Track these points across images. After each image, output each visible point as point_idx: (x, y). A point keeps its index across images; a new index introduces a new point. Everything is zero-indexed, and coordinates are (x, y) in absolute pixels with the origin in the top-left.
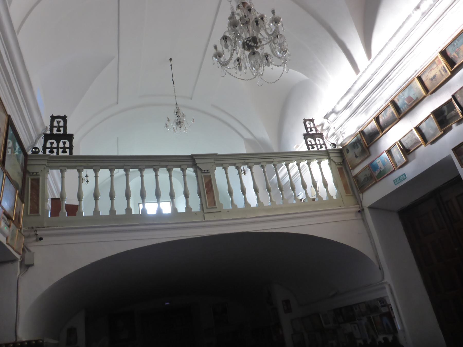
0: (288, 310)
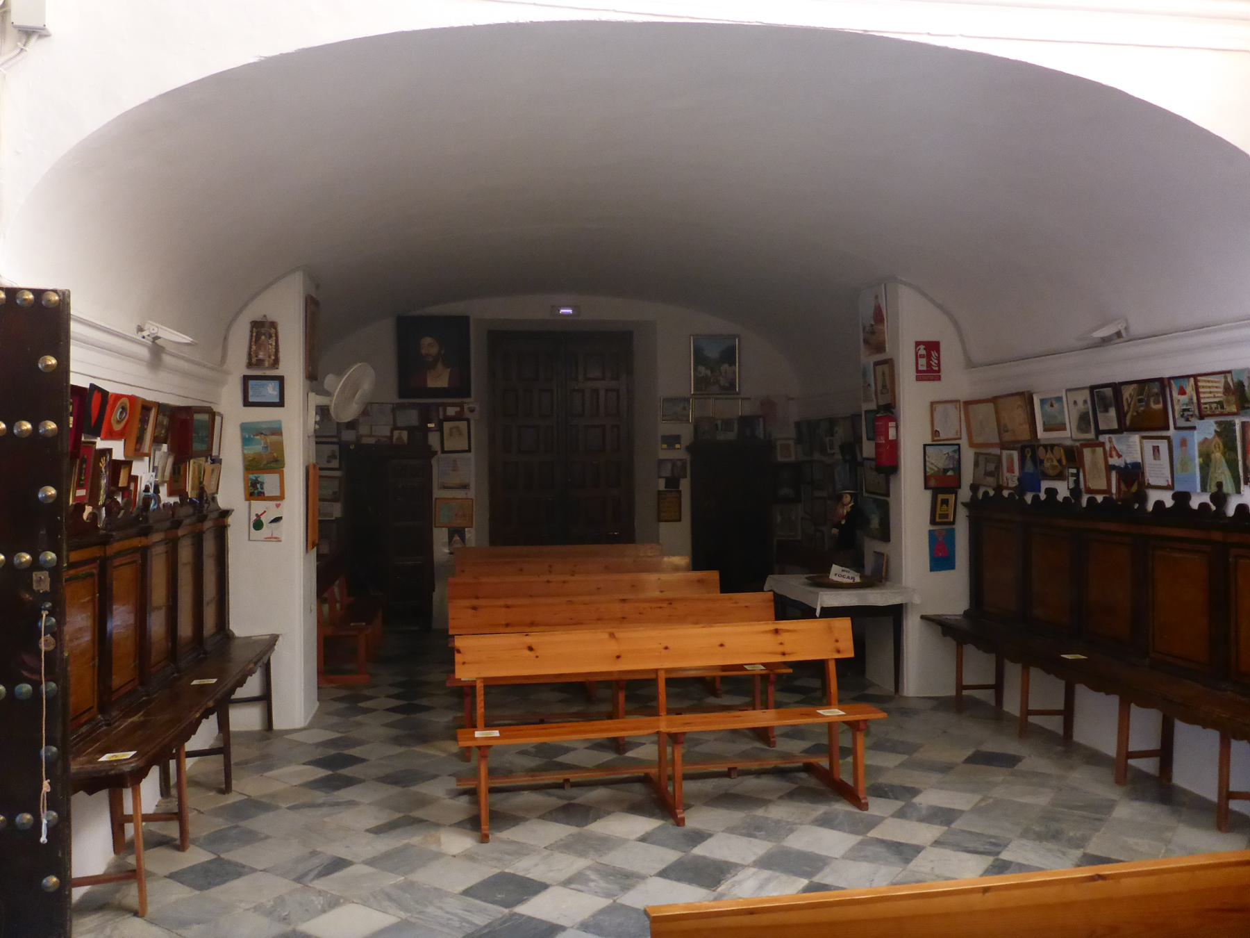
0: (930, 373)
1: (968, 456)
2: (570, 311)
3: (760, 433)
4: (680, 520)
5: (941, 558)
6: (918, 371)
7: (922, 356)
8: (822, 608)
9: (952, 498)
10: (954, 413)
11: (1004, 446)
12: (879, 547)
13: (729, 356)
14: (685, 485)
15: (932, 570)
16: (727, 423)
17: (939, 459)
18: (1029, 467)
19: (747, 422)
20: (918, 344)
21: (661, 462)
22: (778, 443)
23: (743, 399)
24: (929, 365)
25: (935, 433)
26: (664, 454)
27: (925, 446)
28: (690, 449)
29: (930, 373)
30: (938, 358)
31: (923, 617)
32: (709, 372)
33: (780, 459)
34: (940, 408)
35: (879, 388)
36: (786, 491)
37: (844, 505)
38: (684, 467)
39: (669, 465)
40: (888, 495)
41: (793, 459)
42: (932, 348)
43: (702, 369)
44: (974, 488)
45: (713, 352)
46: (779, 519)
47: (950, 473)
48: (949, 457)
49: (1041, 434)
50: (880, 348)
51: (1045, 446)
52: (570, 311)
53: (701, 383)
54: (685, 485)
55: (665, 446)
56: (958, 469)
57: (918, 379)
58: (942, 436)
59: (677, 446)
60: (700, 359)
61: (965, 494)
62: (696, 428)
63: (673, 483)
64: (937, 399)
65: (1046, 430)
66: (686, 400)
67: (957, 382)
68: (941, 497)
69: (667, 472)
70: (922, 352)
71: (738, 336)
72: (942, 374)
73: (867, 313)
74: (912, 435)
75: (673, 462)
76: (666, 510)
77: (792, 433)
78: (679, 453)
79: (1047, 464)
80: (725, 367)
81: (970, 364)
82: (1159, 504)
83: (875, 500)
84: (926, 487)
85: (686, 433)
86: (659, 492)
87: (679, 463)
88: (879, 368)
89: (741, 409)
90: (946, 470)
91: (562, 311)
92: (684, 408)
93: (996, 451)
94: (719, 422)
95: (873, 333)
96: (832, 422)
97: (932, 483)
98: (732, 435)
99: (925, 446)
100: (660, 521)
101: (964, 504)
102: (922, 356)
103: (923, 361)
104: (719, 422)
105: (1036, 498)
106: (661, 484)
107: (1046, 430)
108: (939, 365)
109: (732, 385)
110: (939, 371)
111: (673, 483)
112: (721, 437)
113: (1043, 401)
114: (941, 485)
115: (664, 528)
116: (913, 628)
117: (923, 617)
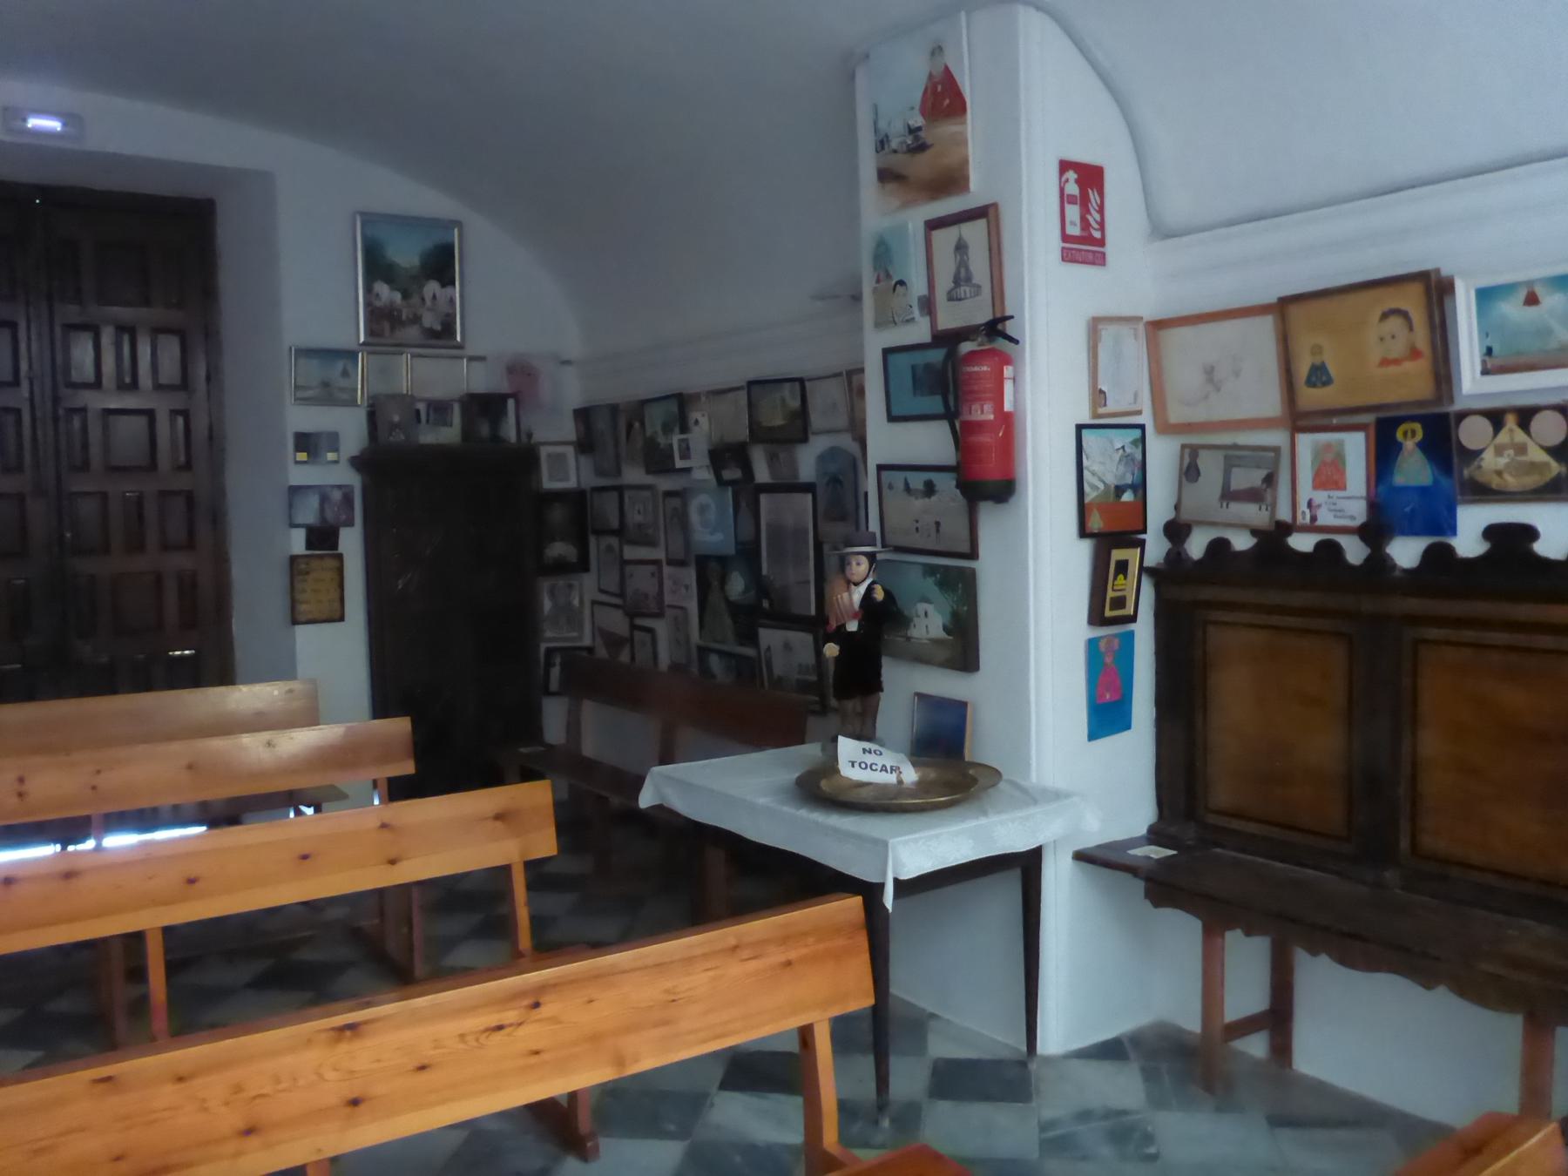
0: (1085, 246)
1: (1162, 456)
2: (54, 125)
3: (510, 432)
4: (342, 619)
5: (1107, 715)
6: (1065, 238)
7: (1072, 199)
8: (898, 883)
9: (1132, 555)
10: (1134, 349)
11: (1298, 420)
12: (945, 684)
13: (440, 265)
14: (351, 542)
15: (1093, 735)
16: (439, 409)
17: (1106, 468)
18: (1414, 469)
19: (485, 406)
20: (1065, 166)
21: (295, 491)
22: (544, 452)
23: (471, 359)
24: (1085, 224)
25: (1098, 397)
26: (301, 474)
27: (1080, 428)
28: (358, 463)
29: (1085, 246)
30: (1101, 210)
31: (1080, 856)
32: (398, 297)
33: (549, 483)
34: (1107, 333)
35: (944, 283)
36: (560, 549)
37: (851, 583)
38: (348, 500)
39: (314, 501)
40: (973, 554)
41: (571, 483)
42: (1090, 177)
43: (382, 289)
44: (1176, 531)
45: (406, 254)
46: (547, 605)
47: (1127, 497)
48: (1127, 458)
49: (1472, 383)
50: (951, 181)
51: (1496, 418)
52: (54, 125)
53: (381, 318)
54: (351, 542)
55: (302, 456)
56: (1140, 487)
57: (1068, 257)
58: (1112, 406)
59: (331, 456)
60: (377, 267)
61: (1156, 548)
62: (372, 416)
63: (323, 538)
64: (1101, 313)
65: (682, 458)
66: (351, 355)
67: (1136, 277)
68: (1117, 555)
69: (309, 512)
70: (1073, 189)
71: (459, 224)
72: (1110, 249)
73: (893, 95)
74: (1047, 399)
75: (323, 494)
76: (307, 604)
77: (568, 429)
78: (337, 473)
79: (1490, 461)
80: (432, 287)
81: (1161, 231)
82: (1219, 547)
83: (930, 570)
84: (1083, 533)
85: (351, 428)
86: (293, 559)
87: (337, 496)
88: (945, 239)
89: (481, 380)
90: (1119, 490)
91: (34, 122)
92: (345, 374)
93: (1277, 438)
94: (421, 407)
95: (920, 147)
96: (682, 402)
97: (1096, 523)
98: (449, 434)
99: (1080, 428)
100: (295, 622)
101: (1152, 572)
102: (1072, 199)
103: (1073, 212)
104: (421, 407)
105: (1439, 556)
106: (297, 542)
107: (682, 458)
108: (1102, 225)
109: (447, 329)
110: (1101, 242)
111: (323, 538)
112: (430, 436)
113: (1486, 296)
114: (1109, 529)
115: (305, 635)
116: (1060, 884)
117: (1080, 856)
